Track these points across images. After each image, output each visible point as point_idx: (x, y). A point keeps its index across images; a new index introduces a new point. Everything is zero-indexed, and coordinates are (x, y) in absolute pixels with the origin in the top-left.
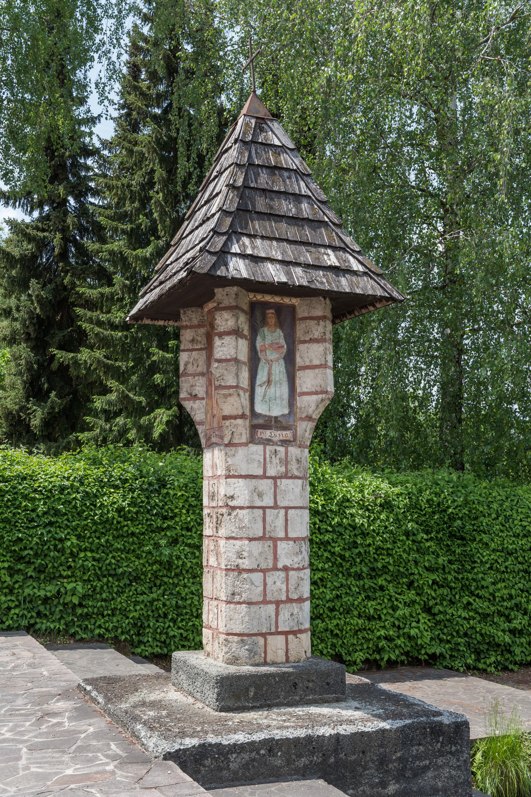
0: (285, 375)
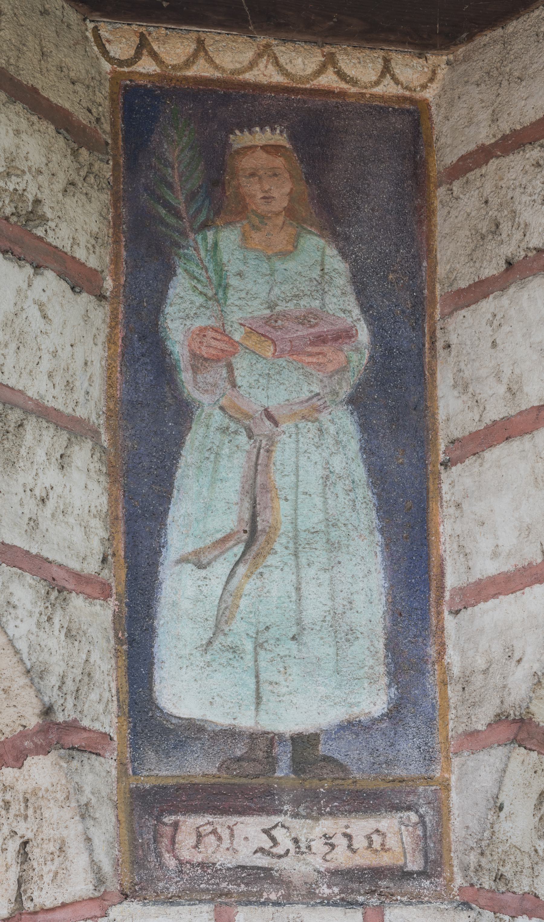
0: (365, 494)
